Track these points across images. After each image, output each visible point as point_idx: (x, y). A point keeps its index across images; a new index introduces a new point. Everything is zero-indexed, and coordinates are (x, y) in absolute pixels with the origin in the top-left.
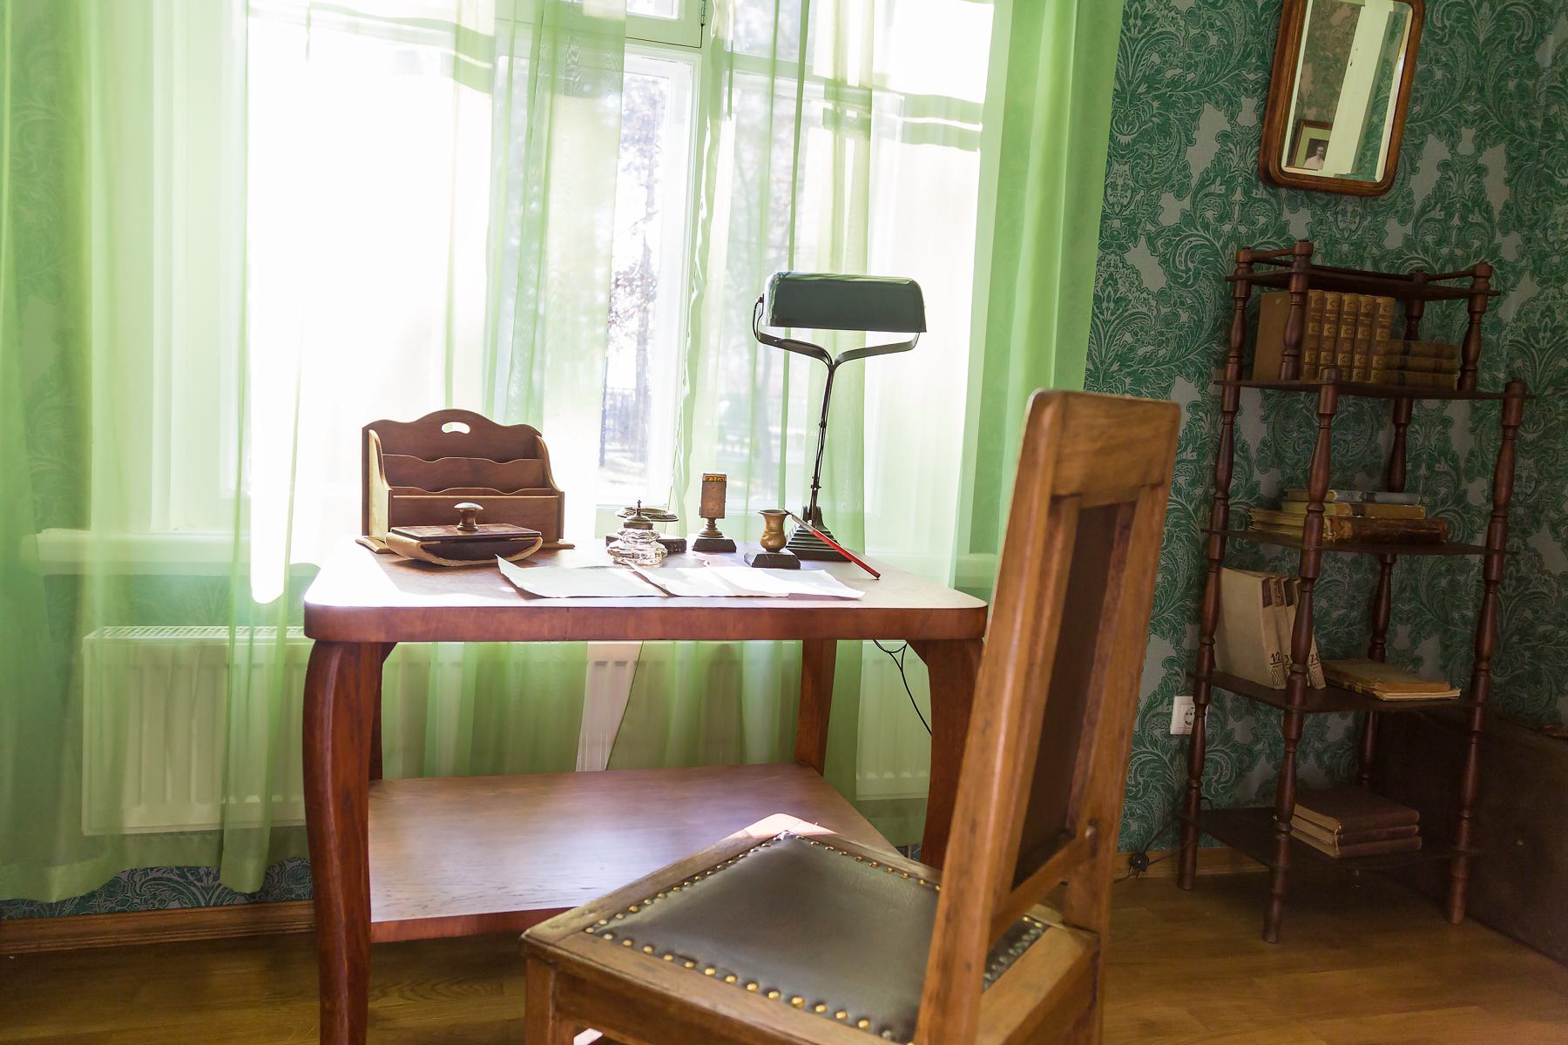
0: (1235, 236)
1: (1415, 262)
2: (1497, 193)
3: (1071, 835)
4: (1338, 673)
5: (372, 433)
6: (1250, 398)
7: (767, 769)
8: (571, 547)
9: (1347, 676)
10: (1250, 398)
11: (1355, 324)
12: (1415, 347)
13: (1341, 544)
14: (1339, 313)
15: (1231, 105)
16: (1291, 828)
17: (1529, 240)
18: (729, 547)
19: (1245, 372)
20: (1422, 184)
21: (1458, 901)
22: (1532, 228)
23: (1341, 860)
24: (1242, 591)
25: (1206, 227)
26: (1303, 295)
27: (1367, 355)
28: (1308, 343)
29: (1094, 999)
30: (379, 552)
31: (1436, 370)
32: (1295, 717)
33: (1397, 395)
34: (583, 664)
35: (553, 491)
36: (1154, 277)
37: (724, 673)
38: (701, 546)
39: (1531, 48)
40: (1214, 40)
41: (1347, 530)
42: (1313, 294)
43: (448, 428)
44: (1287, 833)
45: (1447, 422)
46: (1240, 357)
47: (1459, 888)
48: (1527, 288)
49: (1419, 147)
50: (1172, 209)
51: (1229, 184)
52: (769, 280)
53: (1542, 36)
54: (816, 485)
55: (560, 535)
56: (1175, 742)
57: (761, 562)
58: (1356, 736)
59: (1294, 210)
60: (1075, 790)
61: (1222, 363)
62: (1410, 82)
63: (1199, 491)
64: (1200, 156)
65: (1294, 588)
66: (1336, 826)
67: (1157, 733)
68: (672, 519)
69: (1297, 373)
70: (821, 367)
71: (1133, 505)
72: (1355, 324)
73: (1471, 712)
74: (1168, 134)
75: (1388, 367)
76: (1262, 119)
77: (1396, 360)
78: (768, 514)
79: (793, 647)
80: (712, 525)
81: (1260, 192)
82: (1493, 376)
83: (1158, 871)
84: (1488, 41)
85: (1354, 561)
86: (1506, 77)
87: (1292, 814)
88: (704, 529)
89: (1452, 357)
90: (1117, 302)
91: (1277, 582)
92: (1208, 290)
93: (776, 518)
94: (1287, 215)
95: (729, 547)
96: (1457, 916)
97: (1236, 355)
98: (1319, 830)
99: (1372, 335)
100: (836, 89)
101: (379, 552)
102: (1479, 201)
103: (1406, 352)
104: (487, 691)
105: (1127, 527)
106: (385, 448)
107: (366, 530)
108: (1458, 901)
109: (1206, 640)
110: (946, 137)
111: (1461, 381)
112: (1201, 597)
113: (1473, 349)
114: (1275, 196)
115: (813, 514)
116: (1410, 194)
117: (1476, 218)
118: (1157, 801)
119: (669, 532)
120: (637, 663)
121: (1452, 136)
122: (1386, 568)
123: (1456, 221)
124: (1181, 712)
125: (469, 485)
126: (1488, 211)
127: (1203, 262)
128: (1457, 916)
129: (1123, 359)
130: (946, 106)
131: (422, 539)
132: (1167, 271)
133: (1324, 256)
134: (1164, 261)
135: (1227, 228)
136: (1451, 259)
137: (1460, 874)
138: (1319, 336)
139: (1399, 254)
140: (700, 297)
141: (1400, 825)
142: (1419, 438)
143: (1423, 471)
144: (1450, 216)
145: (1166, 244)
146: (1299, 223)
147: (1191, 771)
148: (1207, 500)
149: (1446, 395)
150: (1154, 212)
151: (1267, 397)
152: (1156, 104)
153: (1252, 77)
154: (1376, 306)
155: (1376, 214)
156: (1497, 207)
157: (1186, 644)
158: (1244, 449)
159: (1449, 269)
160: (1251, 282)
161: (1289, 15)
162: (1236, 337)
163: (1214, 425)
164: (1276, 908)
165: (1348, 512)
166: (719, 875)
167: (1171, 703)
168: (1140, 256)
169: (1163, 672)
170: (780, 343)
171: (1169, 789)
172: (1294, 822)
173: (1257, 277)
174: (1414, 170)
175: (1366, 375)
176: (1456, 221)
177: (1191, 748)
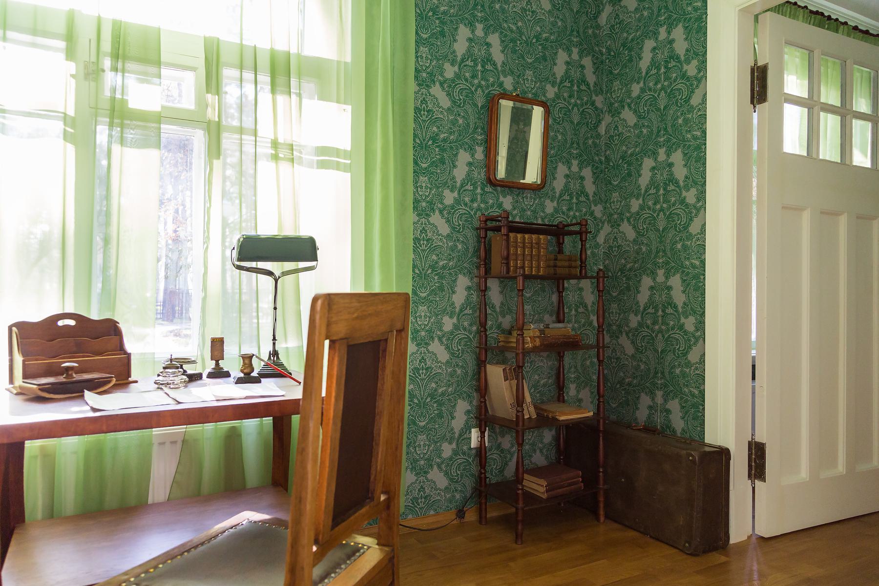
0: (479, 209)
1: (559, 219)
2: (590, 188)
3: (372, 499)
4: (542, 410)
5: (14, 329)
6: (494, 286)
7: (256, 490)
8: (136, 382)
9: (546, 411)
10: (494, 286)
11: (532, 248)
12: (559, 257)
13: (535, 349)
14: (524, 243)
15: (471, 150)
16: (523, 486)
17: (605, 208)
18: (227, 375)
19: (488, 271)
20: (559, 184)
21: (602, 512)
22: (606, 202)
23: (548, 499)
24: (495, 373)
25: (466, 205)
26: (507, 235)
27: (538, 261)
28: (512, 257)
29: (393, 580)
30: (16, 394)
31: (570, 267)
32: (520, 433)
33: (556, 279)
34: (150, 445)
35: (125, 353)
36: (444, 229)
37: (233, 439)
38: (211, 376)
39: (596, 126)
40: (461, 121)
41: (538, 342)
42: (512, 235)
43: (61, 323)
44: (522, 489)
45: (581, 289)
46: (485, 264)
47: (602, 505)
48: (606, 229)
49: (555, 168)
50: (449, 198)
51: (474, 185)
52: (238, 236)
53: (600, 121)
54: (274, 339)
55: (129, 376)
56: (474, 452)
57: (239, 381)
58: (557, 439)
59: (504, 197)
60: (372, 477)
61: (478, 268)
62: (547, 141)
63: (474, 328)
64: (460, 173)
65: (516, 373)
66: (544, 483)
67: (465, 448)
68: (194, 362)
69: (508, 272)
70: (270, 280)
71: (386, 340)
72: (532, 248)
73: (598, 421)
74: (444, 163)
75: (549, 266)
76: (486, 156)
77: (552, 263)
78: (244, 357)
79: (268, 421)
80: (217, 364)
81: (489, 189)
82: (594, 267)
83: (471, 516)
84: (578, 123)
85: (548, 356)
86: (587, 138)
87: (523, 479)
88: (213, 366)
89: (575, 261)
90: (427, 240)
91: (510, 369)
92: (470, 234)
93: (248, 359)
94: (501, 199)
95: (227, 375)
96: (602, 519)
97: (485, 265)
98: (537, 486)
99: (539, 252)
100: (275, 144)
101: (16, 394)
102: (583, 192)
103: (556, 259)
104: (93, 463)
105: (385, 350)
106: (21, 337)
107: (11, 381)
108: (602, 512)
109: (482, 400)
110: (338, 167)
111: (581, 272)
112: (479, 380)
113: (584, 257)
114: (496, 190)
115: (275, 353)
116: (554, 189)
117: (582, 199)
118: (469, 483)
119: (190, 369)
120: (183, 441)
121: (568, 164)
122: (561, 358)
123: (574, 200)
124: (475, 434)
125: (71, 354)
126: (587, 195)
127: (466, 221)
128: (602, 519)
129: (433, 267)
130: (337, 152)
131: (39, 385)
132: (450, 226)
133: (520, 217)
134: (448, 221)
135: (475, 205)
136: (575, 217)
137: (601, 499)
138: (516, 254)
139: (552, 215)
140: (207, 247)
141: (574, 478)
142: (570, 297)
143: (573, 312)
144: (658, 190)
145: (448, 213)
146: (507, 202)
147: (481, 465)
148: (479, 332)
149: (580, 277)
150: (440, 327)
151: (501, 282)
152: (437, 150)
153: (479, 138)
154: (539, 239)
155: (540, 198)
156: (591, 194)
157: (475, 403)
158: (493, 307)
159: (574, 221)
160: (487, 230)
161: (492, 111)
162: (483, 254)
163: (478, 296)
164: (520, 527)
165: (538, 334)
166: (208, 545)
167: (470, 432)
168: (436, 219)
169: (465, 418)
170: (248, 269)
171: (472, 475)
172: (525, 483)
173: (491, 227)
174: (555, 178)
175: (539, 271)
176: (574, 200)
177: (481, 452)
